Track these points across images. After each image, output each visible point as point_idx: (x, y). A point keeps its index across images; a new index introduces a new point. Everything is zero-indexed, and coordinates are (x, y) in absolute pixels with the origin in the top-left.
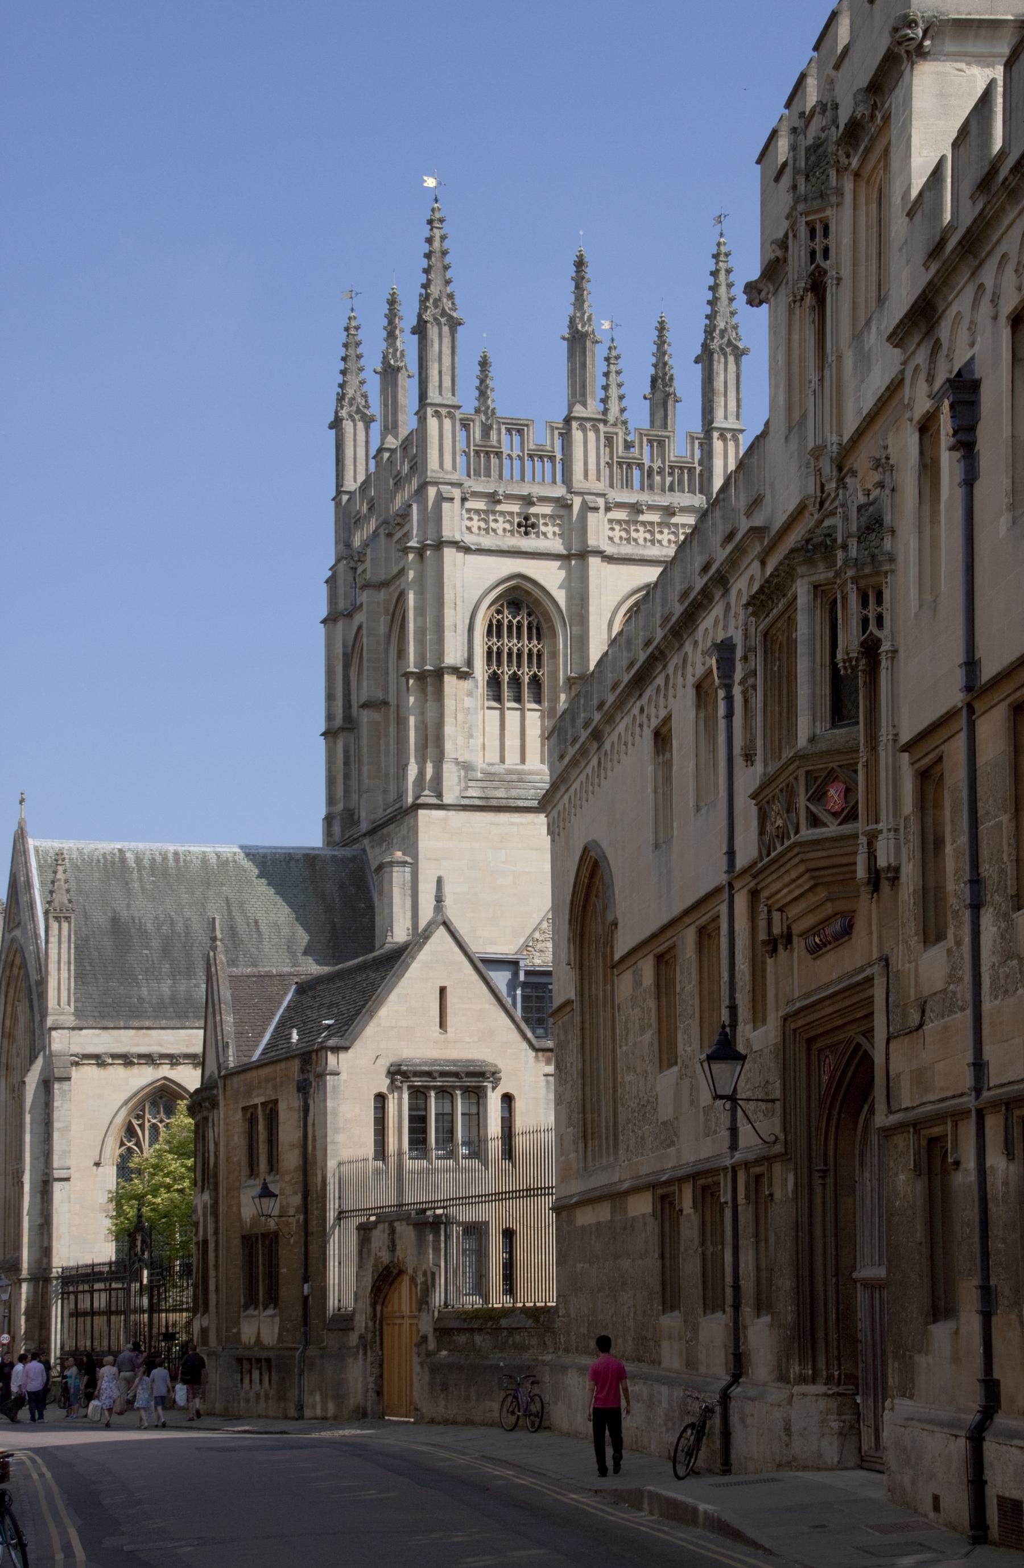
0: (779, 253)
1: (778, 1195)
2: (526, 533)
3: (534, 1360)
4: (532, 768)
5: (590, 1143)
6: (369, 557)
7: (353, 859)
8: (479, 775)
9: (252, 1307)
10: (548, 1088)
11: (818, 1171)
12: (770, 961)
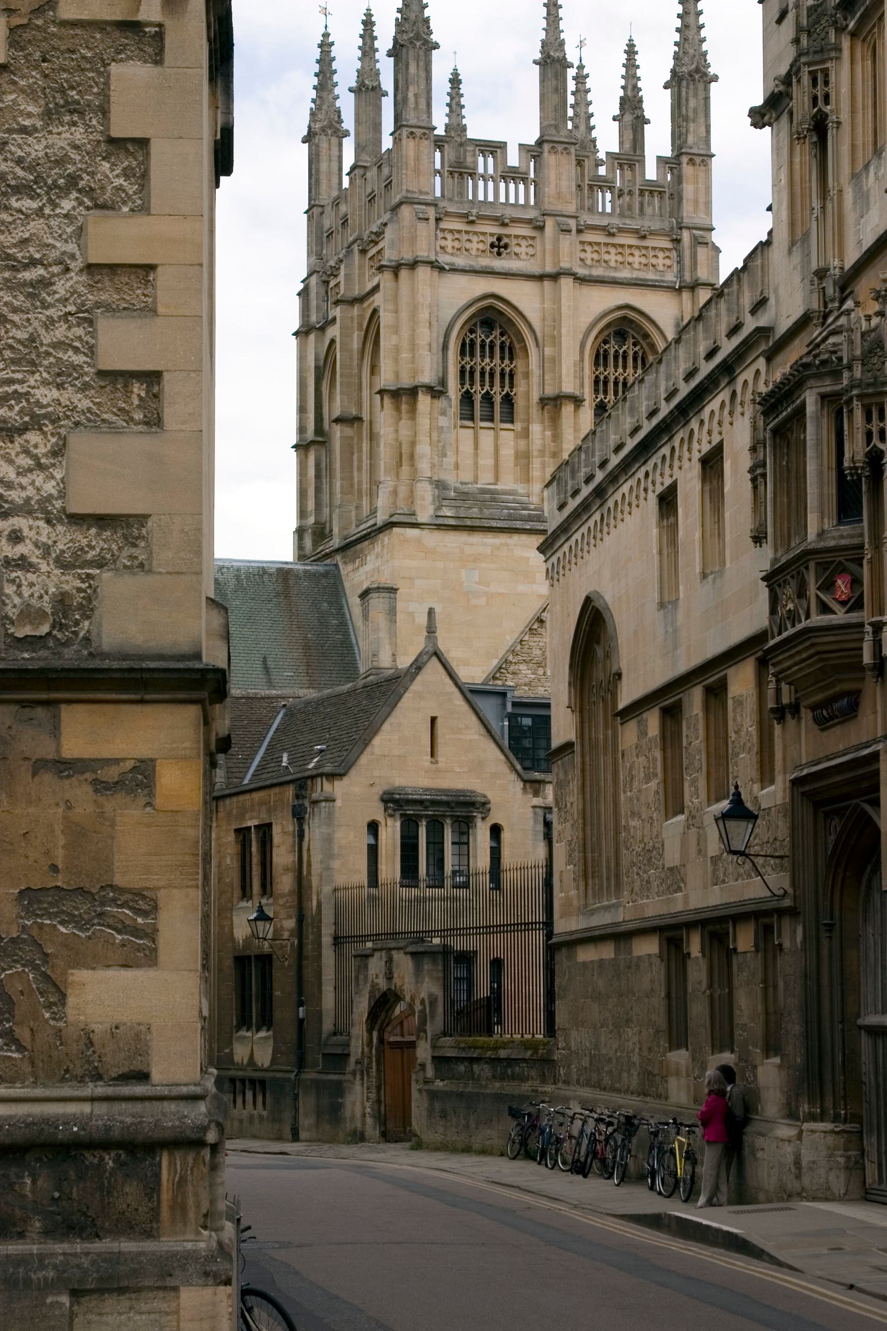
0: (782, 88)
1: (787, 944)
2: (499, 254)
3: (533, 1091)
4: (504, 487)
5: (590, 882)
6: (342, 272)
7: (326, 575)
8: (452, 494)
9: (245, 1028)
10: (535, 820)
11: (825, 925)
12: (777, 729)
